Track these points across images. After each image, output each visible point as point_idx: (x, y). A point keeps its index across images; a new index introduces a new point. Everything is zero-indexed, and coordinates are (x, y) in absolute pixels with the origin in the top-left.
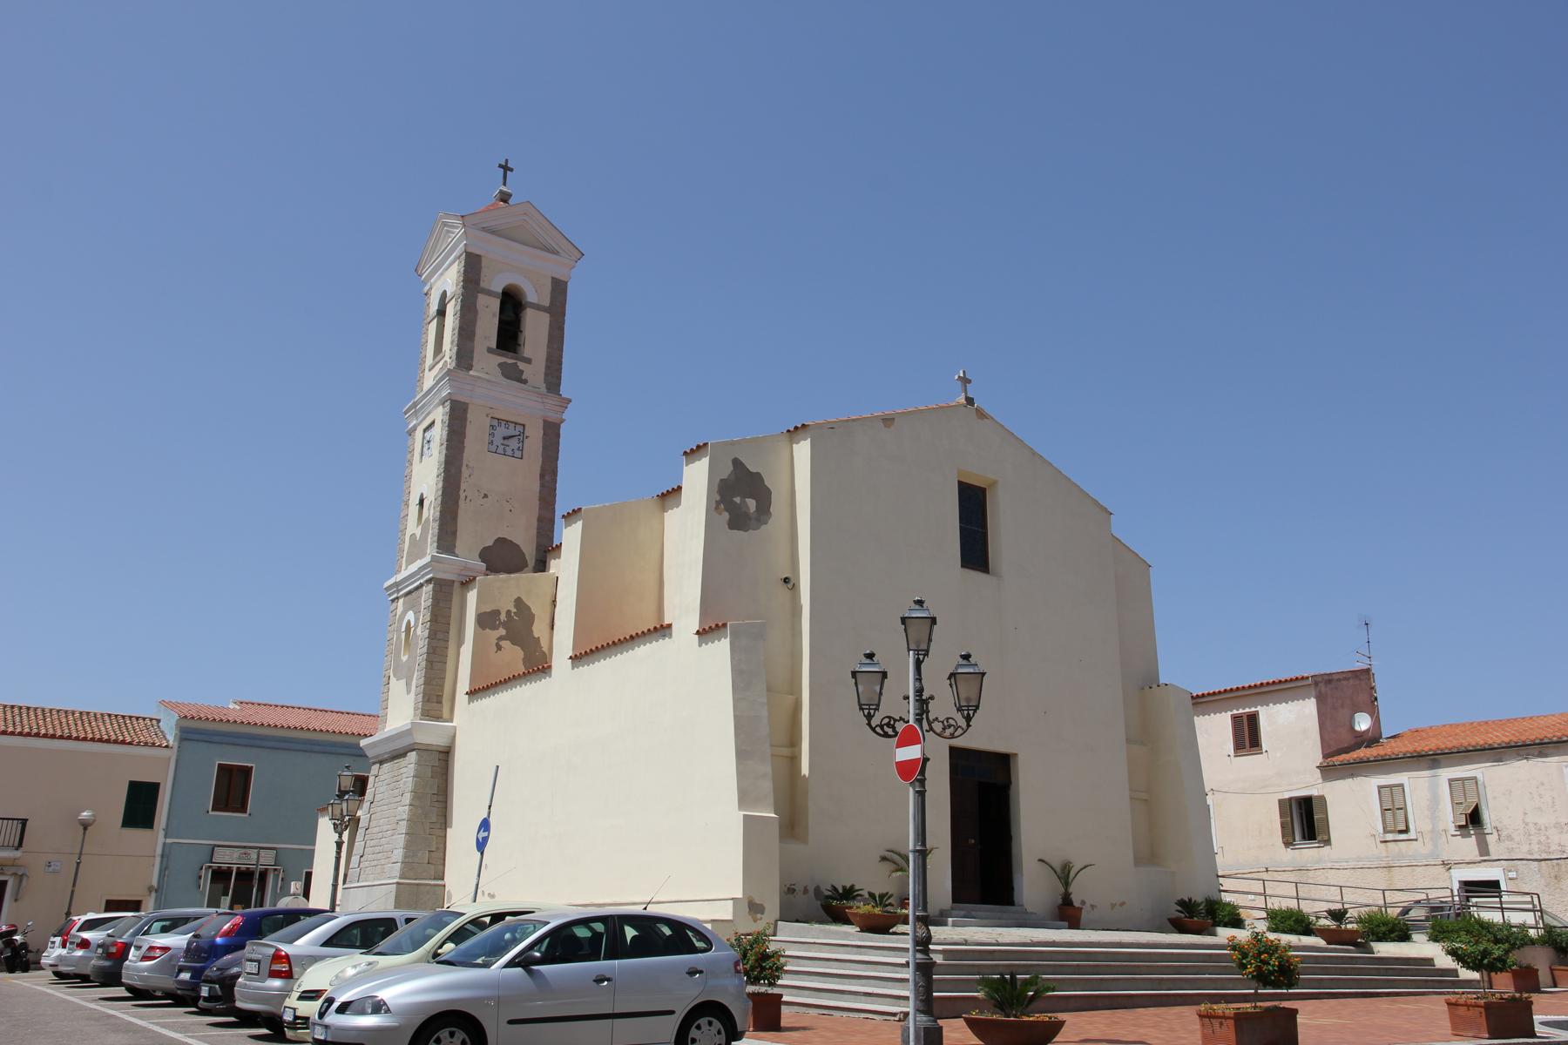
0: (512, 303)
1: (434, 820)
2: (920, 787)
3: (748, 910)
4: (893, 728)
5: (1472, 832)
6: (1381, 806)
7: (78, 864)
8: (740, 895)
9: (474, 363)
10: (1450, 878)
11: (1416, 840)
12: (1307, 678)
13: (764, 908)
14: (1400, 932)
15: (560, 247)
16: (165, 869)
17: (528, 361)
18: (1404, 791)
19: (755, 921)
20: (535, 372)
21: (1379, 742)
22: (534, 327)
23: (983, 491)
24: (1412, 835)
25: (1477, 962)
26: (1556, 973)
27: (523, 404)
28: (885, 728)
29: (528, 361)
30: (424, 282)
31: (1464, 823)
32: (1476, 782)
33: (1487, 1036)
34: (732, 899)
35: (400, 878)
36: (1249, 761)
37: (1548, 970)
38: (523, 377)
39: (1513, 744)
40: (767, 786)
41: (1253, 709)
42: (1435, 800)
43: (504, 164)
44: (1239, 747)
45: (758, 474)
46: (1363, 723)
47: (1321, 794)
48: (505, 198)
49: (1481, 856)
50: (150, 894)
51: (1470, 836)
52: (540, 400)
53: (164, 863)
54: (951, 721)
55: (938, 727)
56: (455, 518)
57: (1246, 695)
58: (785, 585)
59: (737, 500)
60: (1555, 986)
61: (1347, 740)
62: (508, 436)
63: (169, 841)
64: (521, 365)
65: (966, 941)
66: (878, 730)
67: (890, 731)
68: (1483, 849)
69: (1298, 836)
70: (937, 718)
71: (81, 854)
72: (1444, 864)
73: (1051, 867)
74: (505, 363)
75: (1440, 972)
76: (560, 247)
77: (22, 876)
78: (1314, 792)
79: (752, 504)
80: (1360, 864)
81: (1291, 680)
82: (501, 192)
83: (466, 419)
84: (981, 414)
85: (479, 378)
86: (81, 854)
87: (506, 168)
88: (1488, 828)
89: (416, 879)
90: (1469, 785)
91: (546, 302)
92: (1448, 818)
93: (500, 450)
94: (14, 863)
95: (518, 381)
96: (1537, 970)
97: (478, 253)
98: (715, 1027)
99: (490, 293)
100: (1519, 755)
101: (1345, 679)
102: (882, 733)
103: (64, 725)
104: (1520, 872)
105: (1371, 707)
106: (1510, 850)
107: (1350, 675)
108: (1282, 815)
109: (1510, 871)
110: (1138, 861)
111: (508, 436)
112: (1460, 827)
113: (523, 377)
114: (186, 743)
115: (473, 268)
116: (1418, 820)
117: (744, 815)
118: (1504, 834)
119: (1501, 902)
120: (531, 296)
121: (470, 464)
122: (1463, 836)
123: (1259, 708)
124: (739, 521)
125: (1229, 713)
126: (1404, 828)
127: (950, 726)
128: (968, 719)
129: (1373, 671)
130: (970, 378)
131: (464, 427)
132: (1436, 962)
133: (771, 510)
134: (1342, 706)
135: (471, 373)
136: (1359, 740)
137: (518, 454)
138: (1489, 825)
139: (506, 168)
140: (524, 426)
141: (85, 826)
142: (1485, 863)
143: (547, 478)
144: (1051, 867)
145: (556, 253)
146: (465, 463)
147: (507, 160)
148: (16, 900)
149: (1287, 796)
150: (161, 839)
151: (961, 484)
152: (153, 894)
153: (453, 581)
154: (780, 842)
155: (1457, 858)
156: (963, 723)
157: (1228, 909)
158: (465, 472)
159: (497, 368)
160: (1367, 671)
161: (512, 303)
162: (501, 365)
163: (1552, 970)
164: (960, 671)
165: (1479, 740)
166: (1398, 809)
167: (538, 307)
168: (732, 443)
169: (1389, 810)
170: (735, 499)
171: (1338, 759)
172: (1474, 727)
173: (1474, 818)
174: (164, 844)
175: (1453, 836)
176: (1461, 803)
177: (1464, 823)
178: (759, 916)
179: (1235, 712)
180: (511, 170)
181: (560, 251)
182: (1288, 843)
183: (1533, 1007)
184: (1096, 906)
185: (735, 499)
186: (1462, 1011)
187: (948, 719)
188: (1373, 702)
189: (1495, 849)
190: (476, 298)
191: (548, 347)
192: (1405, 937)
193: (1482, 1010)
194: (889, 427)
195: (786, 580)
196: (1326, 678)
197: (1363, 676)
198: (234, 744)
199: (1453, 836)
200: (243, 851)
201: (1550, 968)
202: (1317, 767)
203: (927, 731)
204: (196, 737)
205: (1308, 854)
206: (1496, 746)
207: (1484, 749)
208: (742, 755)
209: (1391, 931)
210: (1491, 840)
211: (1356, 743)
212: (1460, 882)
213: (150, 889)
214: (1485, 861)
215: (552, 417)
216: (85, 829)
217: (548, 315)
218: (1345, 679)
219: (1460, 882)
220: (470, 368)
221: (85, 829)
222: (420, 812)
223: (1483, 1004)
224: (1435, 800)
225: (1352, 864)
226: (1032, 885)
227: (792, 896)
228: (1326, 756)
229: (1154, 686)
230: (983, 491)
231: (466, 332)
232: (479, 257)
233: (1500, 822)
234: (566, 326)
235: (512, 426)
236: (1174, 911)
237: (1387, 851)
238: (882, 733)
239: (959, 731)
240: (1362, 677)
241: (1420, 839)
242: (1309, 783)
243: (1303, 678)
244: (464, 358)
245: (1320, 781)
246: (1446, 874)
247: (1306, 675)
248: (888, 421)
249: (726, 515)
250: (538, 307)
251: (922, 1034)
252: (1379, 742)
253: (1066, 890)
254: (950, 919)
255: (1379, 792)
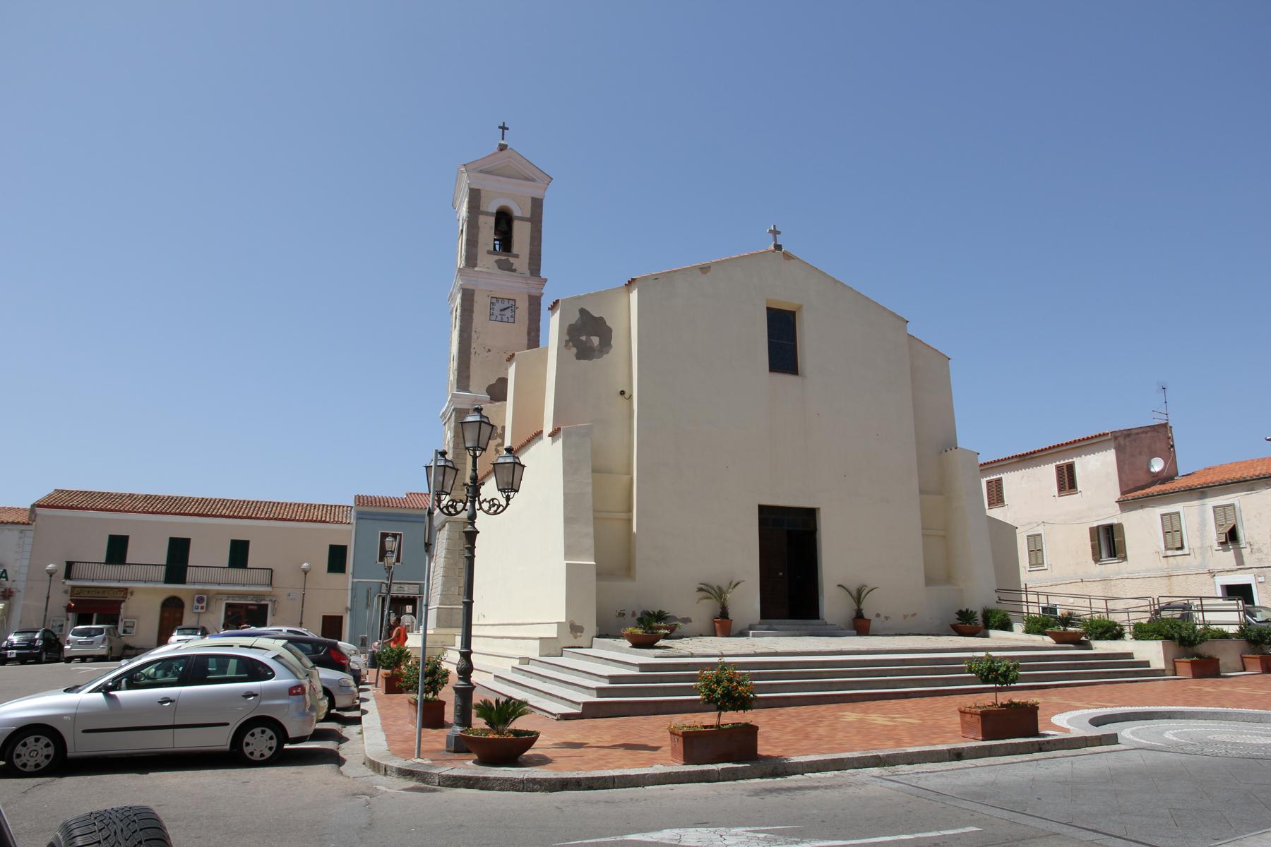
0: (504, 220)
1: (461, 567)
2: (468, 553)
3: (570, 630)
4: (455, 508)
5: (1231, 547)
6: (1163, 530)
7: (304, 594)
8: (564, 620)
9: (478, 262)
10: (1214, 583)
11: (1189, 555)
12: (1108, 434)
13: (583, 629)
14: (1113, 632)
15: (536, 176)
16: (355, 597)
17: (517, 256)
18: (1180, 518)
19: (575, 638)
20: (521, 262)
21: (1173, 479)
22: (521, 233)
23: (793, 313)
24: (1186, 551)
25: (983, 677)
26: (1246, 660)
27: (514, 286)
28: (451, 509)
29: (517, 256)
30: (457, 212)
31: (1224, 540)
32: (1234, 508)
33: (981, 738)
34: (557, 623)
35: (440, 604)
36: (1069, 499)
37: (1239, 658)
38: (514, 268)
39: (1262, 476)
40: (589, 542)
41: (1071, 460)
42: (1203, 524)
43: (502, 125)
44: (1061, 489)
45: (601, 319)
46: (1157, 465)
47: (1119, 522)
48: (503, 148)
49: (1238, 565)
50: (347, 612)
51: (1229, 550)
52: (525, 282)
53: (354, 593)
54: (496, 502)
55: (485, 506)
56: (468, 367)
57: (1062, 451)
58: (623, 397)
59: (583, 338)
60: (1245, 671)
61: (1144, 479)
62: (503, 308)
63: (355, 580)
64: (512, 260)
65: (692, 654)
66: (445, 510)
67: (452, 511)
68: (1239, 559)
69: (1104, 554)
70: (485, 499)
71: (304, 588)
72: (1209, 573)
73: (847, 591)
74: (500, 260)
75: (1131, 664)
76: (536, 176)
77: (275, 601)
78: (1114, 521)
79: (595, 340)
80: (1148, 574)
81: (1096, 436)
82: (500, 145)
83: (473, 300)
84: (788, 256)
85: (481, 272)
86: (304, 588)
87: (503, 128)
88: (1243, 543)
89: (450, 605)
90: (1229, 511)
91: (528, 214)
92: (1213, 536)
93: (499, 319)
94: (270, 594)
95: (510, 271)
96: (1218, 660)
97: (477, 188)
98: (271, 743)
99: (487, 214)
100: (1267, 485)
101: (1144, 432)
102: (447, 512)
103: (295, 512)
104: (1267, 576)
105: (1169, 452)
106: (1260, 560)
107: (1148, 429)
108: (1092, 540)
109: (1260, 576)
110: (930, 581)
111: (503, 308)
112: (1222, 543)
113: (514, 268)
114: (360, 521)
115: (475, 197)
116: (1190, 540)
117: (567, 564)
118: (1255, 547)
119: (1202, 605)
120: (517, 212)
121: (477, 331)
122: (1224, 550)
123: (1075, 459)
124: (585, 353)
125: (1054, 464)
126: (1180, 546)
127: (494, 505)
128: (508, 499)
129: (1170, 425)
130: (779, 230)
131: (472, 306)
132: (1135, 656)
133: (612, 343)
134: (1140, 453)
135: (476, 269)
136: (1156, 479)
137: (511, 320)
138: (1243, 541)
139: (503, 128)
140: (515, 300)
141: (306, 572)
142: (1241, 571)
143: (533, 334)
144: (847, 591)
145: (533, 180)
146: (474, 329)
147: (504, 123)
148: (274, 615)
149: (1095, 525)
150: (350, 580)
151: (769, 309)
152: (349, 612)
153: (469, 409)
154: (597, 580)
155: (1220, 568)
156: (503, 502)
157: (997, 616)
158: (474, 336)
159: (495, 264)
160: (1165, 425)
161: (504, 220)
162: (497, 261)
163: (1242, 658)
164: (499, 462)
165: (1237, 475)
166: (1175, 531)
167: (521, 219)
168: (579, 298)
169: (1169, 532)
170: (582, 338)
171: (1130, 496)
172: (1252, 463)
173: (1232, 536)
174: (353, 582)
175: (1217, 550)
176: (1223, 525)
177: (1224, 540)
178: (579, 634)
179: (1058, 463)
180: (507, 129)
181: (536, 179)
182: (1097, 558)
183: (1038, 712)
184: (890, 617)
185: (582, 338)
186: (968, 717)
187: (493, 500)
188: (1169, 449)
189: (1249, 560)
190: (478, 217)
191: (531, 245)
192: (1118, 636)
193: (979, 717)
194: (705, 273)
195: (622, 393)
196: (1125, 433)
197: (1162, 430)
198: (389, 520)
199: (1217, 550)
200: (399, 585)
201: (1241, 656)
202: (1116, 502)
203: (478, 510)
204: (368, 517)
205: (1111, 567)
206: (1249, 478)
207: (1240, 482)
208: (568, 520)
209: (1106, 632)
210: (1245, 552)
211: (1152, 482)
212: (1222, 586)
213: (347, 609)
214: (1241, 569)
215: (534, 292)
216: (306, 574)
217: (530, 223)
218: (1144, 432)
219: (1222, 586)
220: (475, 265)
221: (306, 574)
222: (452, 561)
223: (979, 713)
224: (1203, 524)
225: (1142, 575)
226: (832, 603)
227: (622, 618)
228: (1123, 493)
229: (953, 449)
230: (793, 313)
231: (472, 243)
232: (479, 190)
233: (1253, 538)
234: (543, 229)
235: (506, 301)
236: (954, 619)
237: (1168, 564)
238: (447, 512)
239: (501, 508)
240: (1159, 430)
241: (1192, 554)
242: (1110, 514)
243: (1104, 434)
244: (471, 260)
245: (1119, 512)
246: (1212, 580)
247: (1107, 432)
248: (704, 269)
249: (574, 350)
250: (521, 219)
251: (453, 741)
252: (1173, 479)
253: (858, 606)
254: (751, 632)
255: (1162, 518)
